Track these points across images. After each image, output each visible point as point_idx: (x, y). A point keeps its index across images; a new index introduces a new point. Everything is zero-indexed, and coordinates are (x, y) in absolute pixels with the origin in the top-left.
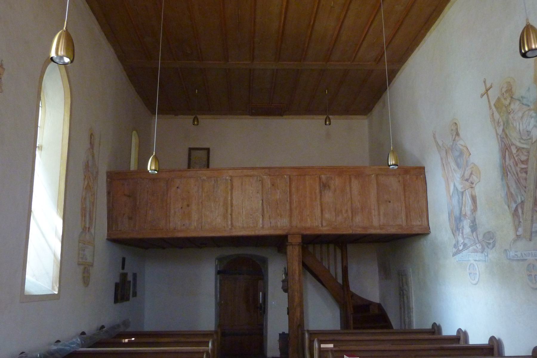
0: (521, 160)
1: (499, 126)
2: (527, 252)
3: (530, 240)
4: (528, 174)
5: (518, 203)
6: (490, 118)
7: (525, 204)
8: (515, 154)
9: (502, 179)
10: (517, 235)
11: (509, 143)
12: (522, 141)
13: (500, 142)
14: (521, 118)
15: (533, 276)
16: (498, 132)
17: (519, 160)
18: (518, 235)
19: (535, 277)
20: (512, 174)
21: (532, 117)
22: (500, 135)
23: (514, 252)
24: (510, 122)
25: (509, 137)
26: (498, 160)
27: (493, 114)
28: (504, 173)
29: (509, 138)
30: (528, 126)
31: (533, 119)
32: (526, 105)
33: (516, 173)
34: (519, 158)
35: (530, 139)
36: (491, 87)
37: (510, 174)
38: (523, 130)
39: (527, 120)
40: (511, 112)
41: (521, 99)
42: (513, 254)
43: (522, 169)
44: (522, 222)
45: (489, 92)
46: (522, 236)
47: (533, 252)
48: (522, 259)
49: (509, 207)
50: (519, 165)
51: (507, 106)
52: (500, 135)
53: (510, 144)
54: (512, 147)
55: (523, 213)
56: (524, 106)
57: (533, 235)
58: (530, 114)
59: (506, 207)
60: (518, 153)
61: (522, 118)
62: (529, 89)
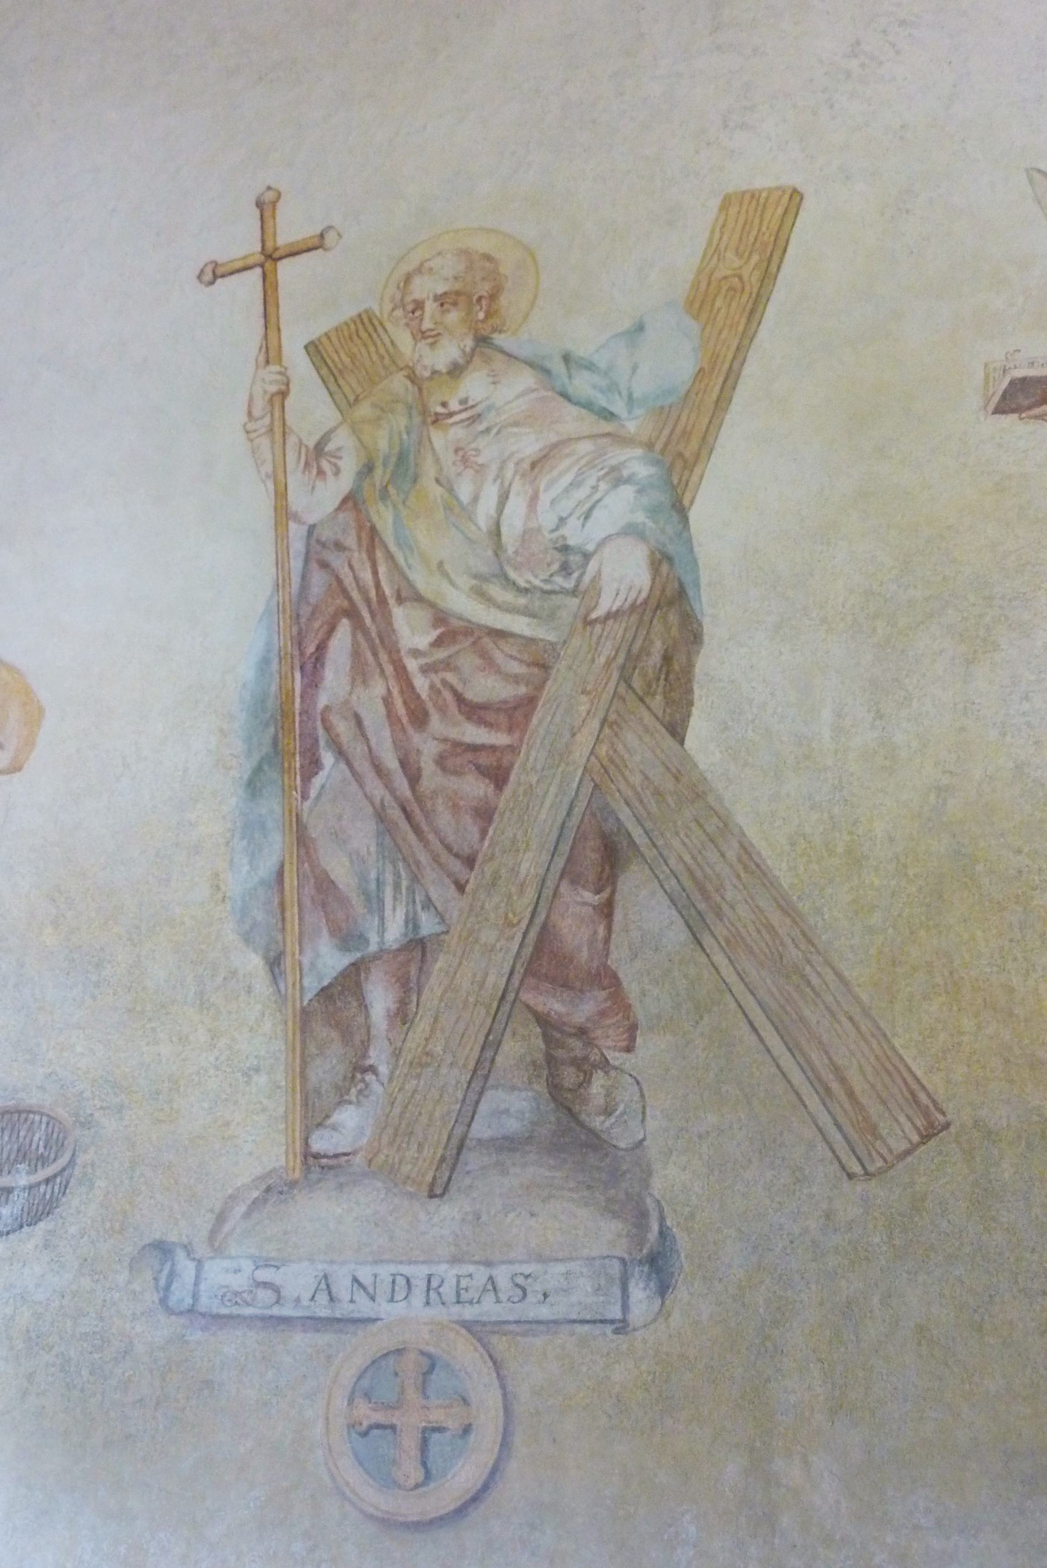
0: (469, 695)
1: (321, 473)
2: (385, 1272)
3: (436, 1192)
4: (508, 790)
5: (373, 948)
6: (250, 414)
7: (440, 963)
8: (416, 653)
9: (253, 786)
10: (309, 1157)
11: (378, 585)
12: (495, 591)
13: (296, 565)
14: (526, 465)
15: (410, 1442)
16: (297, 500)
17: (448, 695)
18: (317, 1156)
19: (424, 1445)
20: (363, 766)
21: (617, 478)
22: (312, 529)
23: (247, 1266)
24: (429, 471)
25: (393, 548)
26: (247, 671)
27: (284, 394)
28: (277, 753)
29: (390, 557)
30: (574, 522)
31: (627, 492)
32: (588, 406)
33: (404, 764)
34: (444, 682)
35: (574, 592)
36: (316, 248)
37: (343, 766)
38: (528, 535)
39: (575, 484)
40: (451, 415)
41: (558, 367)
42: (239, 1282)
43: (460, 747)
44: (383, 1069)
45: (286, 270)
46: (358, 1160)
47: (449, 1273)
48: (324, 1313)
49: (274, 963)
50: (435, 722)
51: (427, 374)
52: (312, 529)
53: (388, 591)
54: (398, 613)
55: (402, 1016)
56: (574, 410)
57: (473, 1159)
58: (613, 462)
59: (254, 962)
60: (441, 654)
61: (533, 465)
62: (640, 328)
